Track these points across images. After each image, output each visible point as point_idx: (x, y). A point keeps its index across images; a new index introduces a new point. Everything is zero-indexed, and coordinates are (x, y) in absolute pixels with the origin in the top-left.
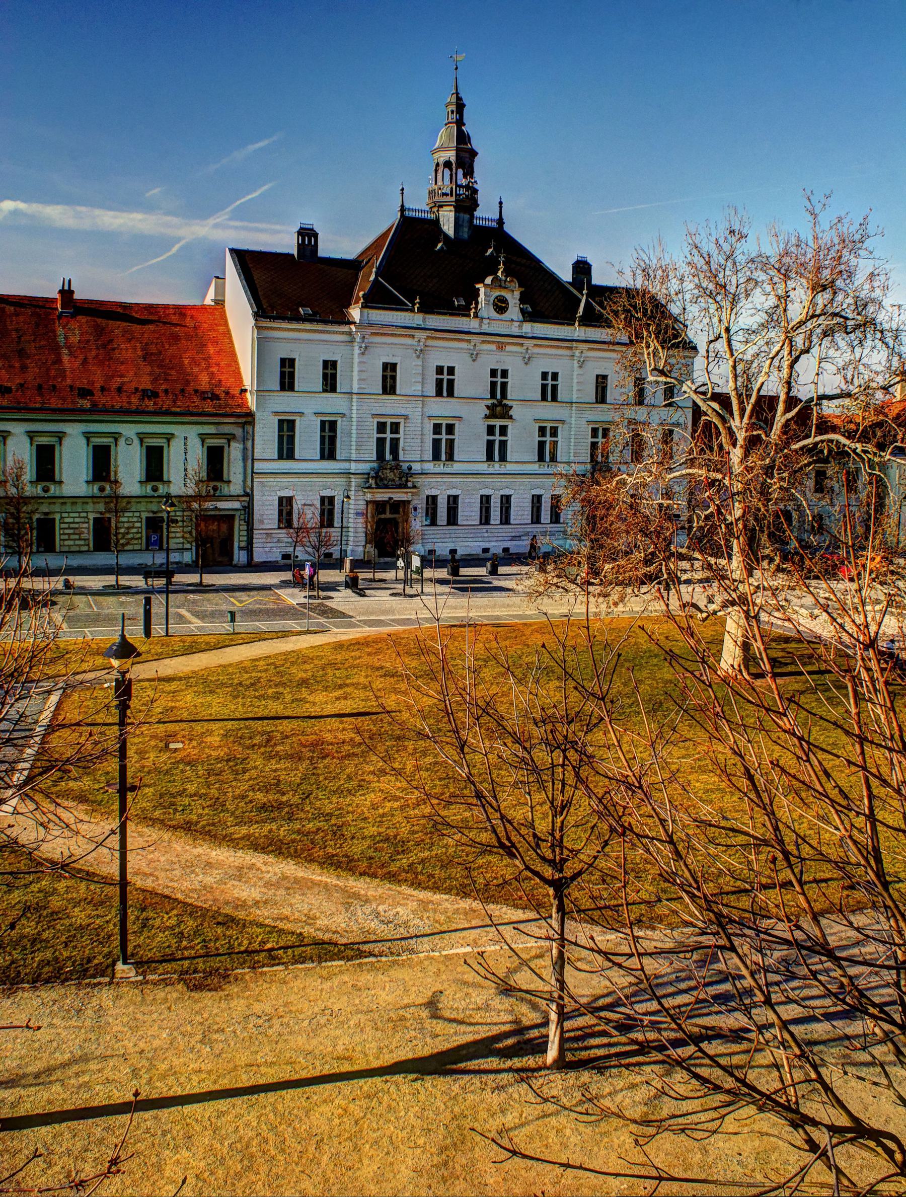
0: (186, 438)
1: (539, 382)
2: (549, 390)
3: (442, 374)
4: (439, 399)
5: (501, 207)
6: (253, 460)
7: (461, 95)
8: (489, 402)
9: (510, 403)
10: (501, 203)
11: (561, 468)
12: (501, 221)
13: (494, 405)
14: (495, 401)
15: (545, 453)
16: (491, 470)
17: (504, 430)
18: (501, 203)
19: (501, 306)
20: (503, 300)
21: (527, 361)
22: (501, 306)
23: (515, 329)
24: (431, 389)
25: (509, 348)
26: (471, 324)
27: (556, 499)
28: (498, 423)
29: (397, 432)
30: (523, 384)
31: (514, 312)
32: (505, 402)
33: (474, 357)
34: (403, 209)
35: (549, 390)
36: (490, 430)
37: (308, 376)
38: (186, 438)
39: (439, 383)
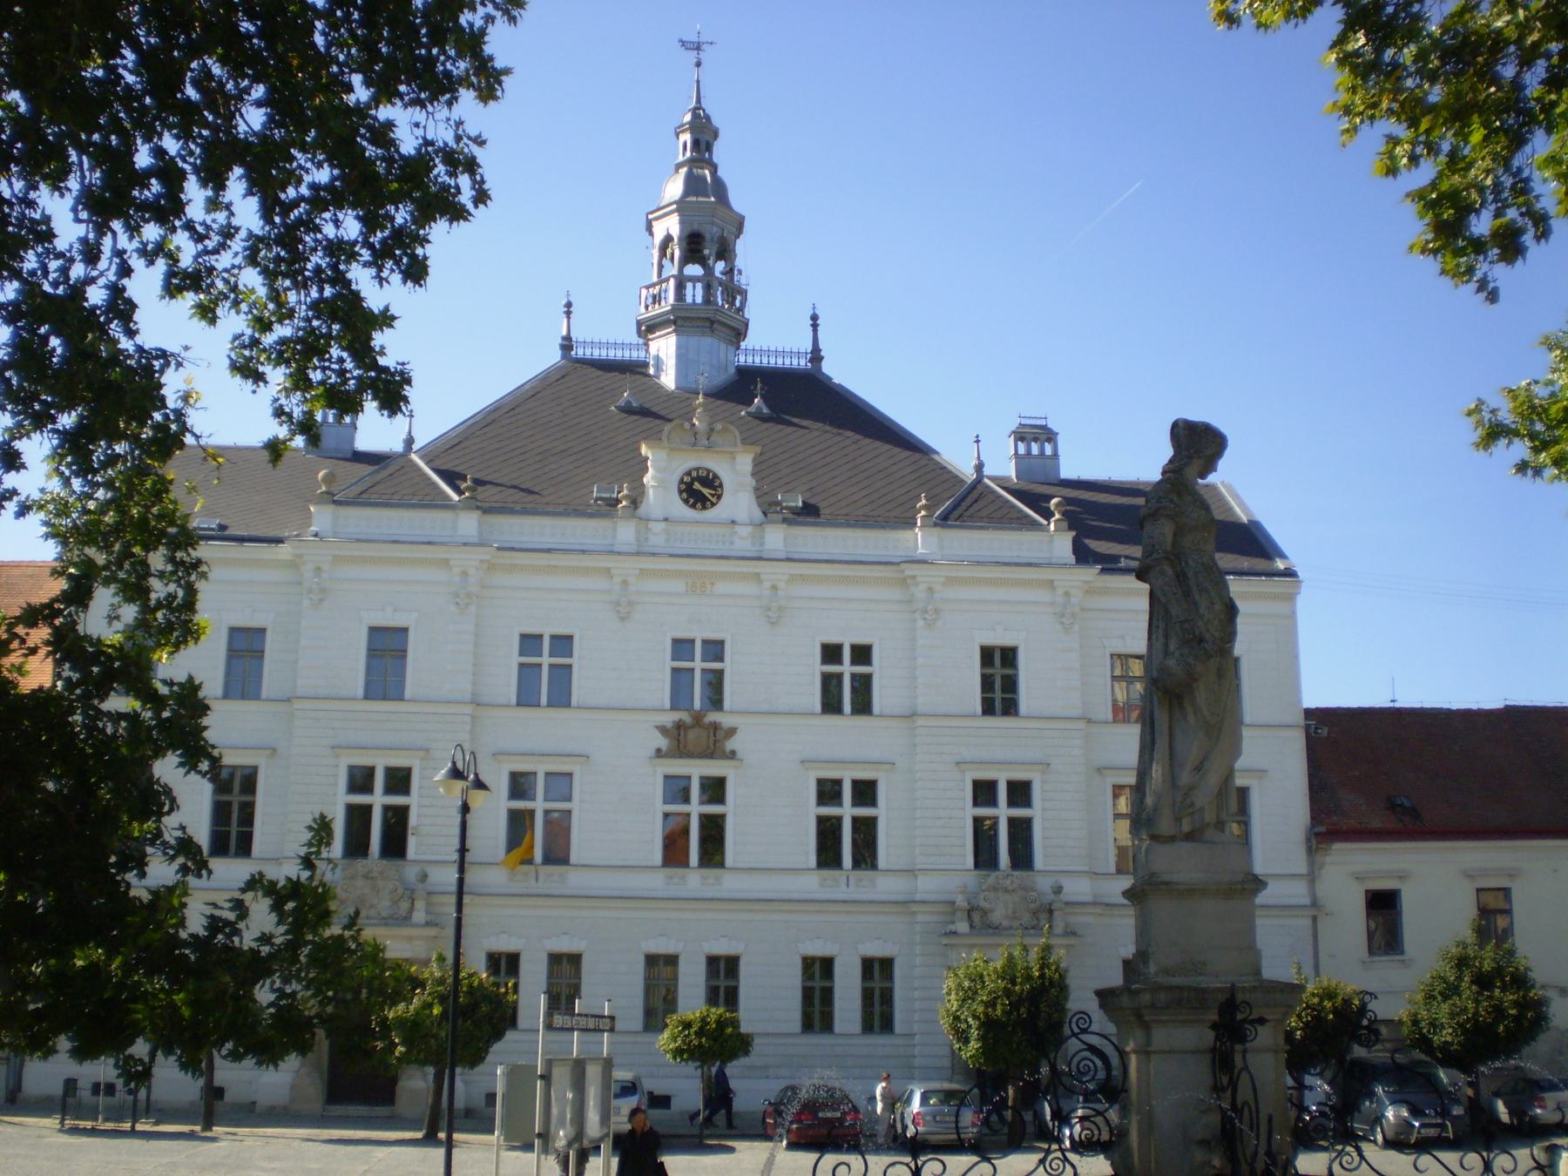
1: (816, 667)
2: (846, 683)
3: (993, 802)
4: (525, 713)
5: (815, 326)
7: (710, 106)
8: (669, 718)
9: (724, 719)
10: (814, 318)
11: (883, 885)
12: (816, 356)
13: (679, 726)
14: (684, 716)
15: (846, 834)
16: (674, 891)
17: (715, 789)
18: (814, 318)
19: (699, 490)
20: (711, 481)
21: (774, 615)
23: (743, 541)
24: (505, 684)
25: (722, 587)
26: (625, 532)
27: (877, 970)
28: (697, 770)
29: (370, 772)
30: (772, 676)
31: (738, 501)
32: (713, 717)
33: (624, 609)
34: (567, 345)
35: (846, 683)
36: (677, 790)
39: (528, 673)
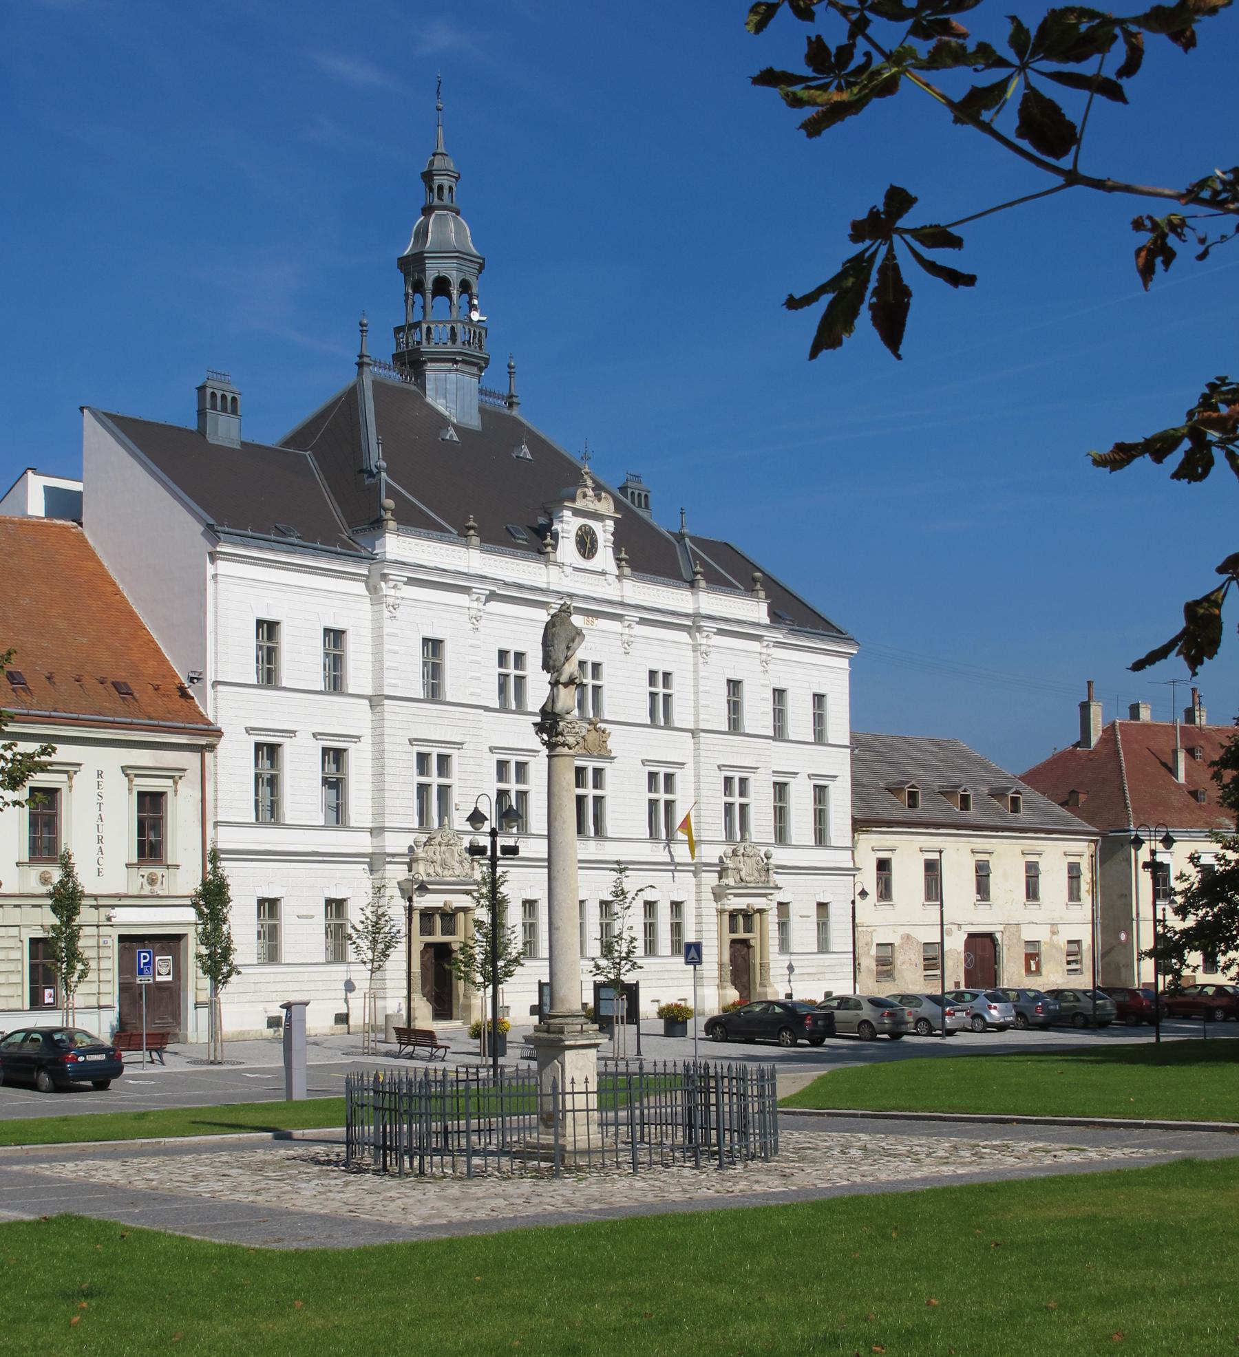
0: (100, 774)
2: (660, 710)
6: (216, 824)
15: (663, 819)
22: (586, 544)
31: (605, 557)
35: (660, 710)
37: (301, 659)
38: (100, 774)
